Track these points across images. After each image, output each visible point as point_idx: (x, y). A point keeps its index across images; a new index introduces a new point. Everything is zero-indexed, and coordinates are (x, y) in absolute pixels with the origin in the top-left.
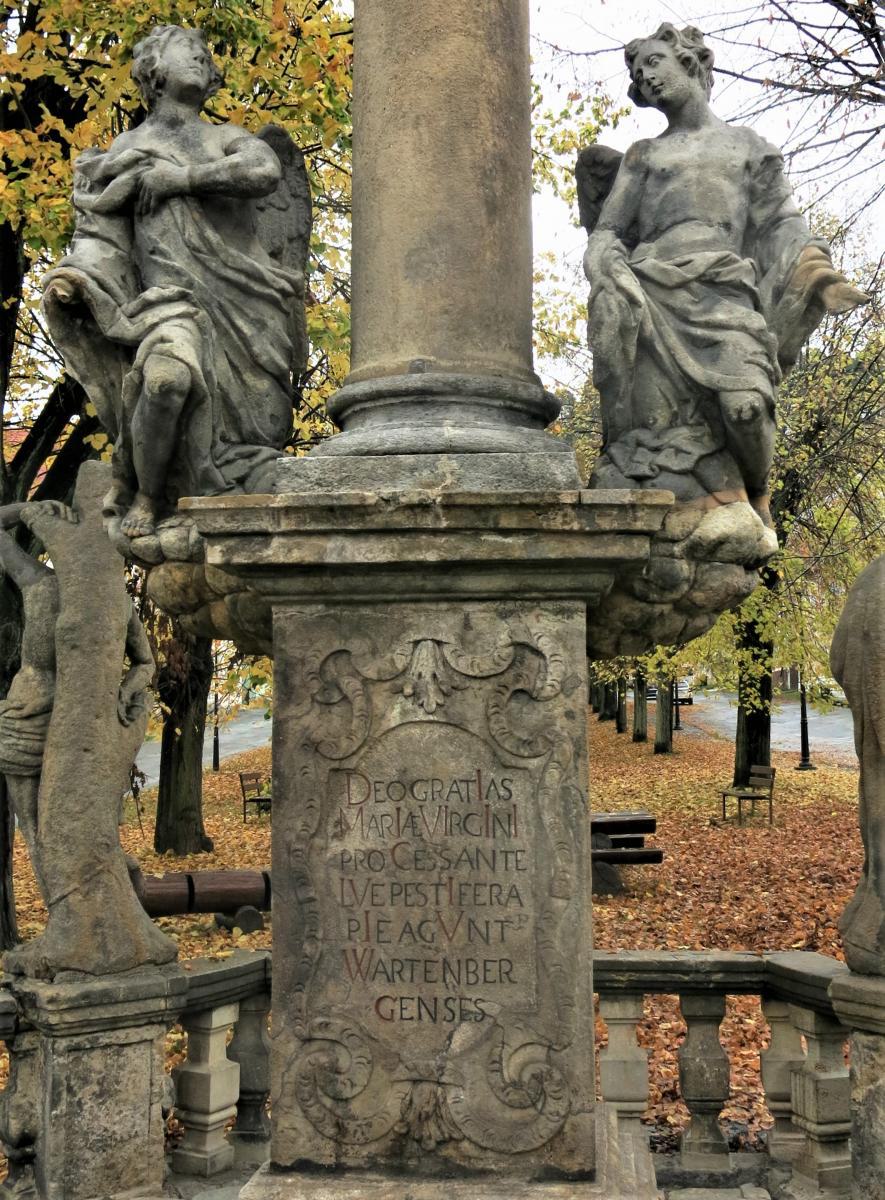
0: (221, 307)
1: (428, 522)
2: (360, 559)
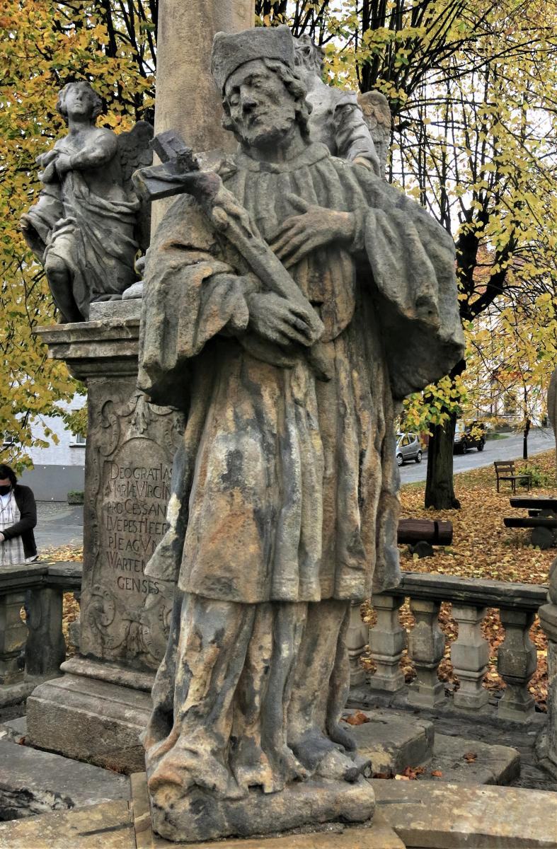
0: (88, 225)
1: (124, 335)
2: (102, 355)
